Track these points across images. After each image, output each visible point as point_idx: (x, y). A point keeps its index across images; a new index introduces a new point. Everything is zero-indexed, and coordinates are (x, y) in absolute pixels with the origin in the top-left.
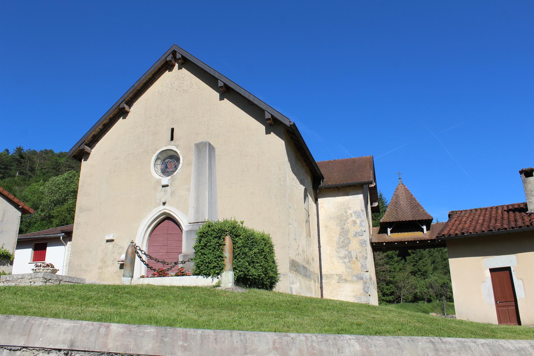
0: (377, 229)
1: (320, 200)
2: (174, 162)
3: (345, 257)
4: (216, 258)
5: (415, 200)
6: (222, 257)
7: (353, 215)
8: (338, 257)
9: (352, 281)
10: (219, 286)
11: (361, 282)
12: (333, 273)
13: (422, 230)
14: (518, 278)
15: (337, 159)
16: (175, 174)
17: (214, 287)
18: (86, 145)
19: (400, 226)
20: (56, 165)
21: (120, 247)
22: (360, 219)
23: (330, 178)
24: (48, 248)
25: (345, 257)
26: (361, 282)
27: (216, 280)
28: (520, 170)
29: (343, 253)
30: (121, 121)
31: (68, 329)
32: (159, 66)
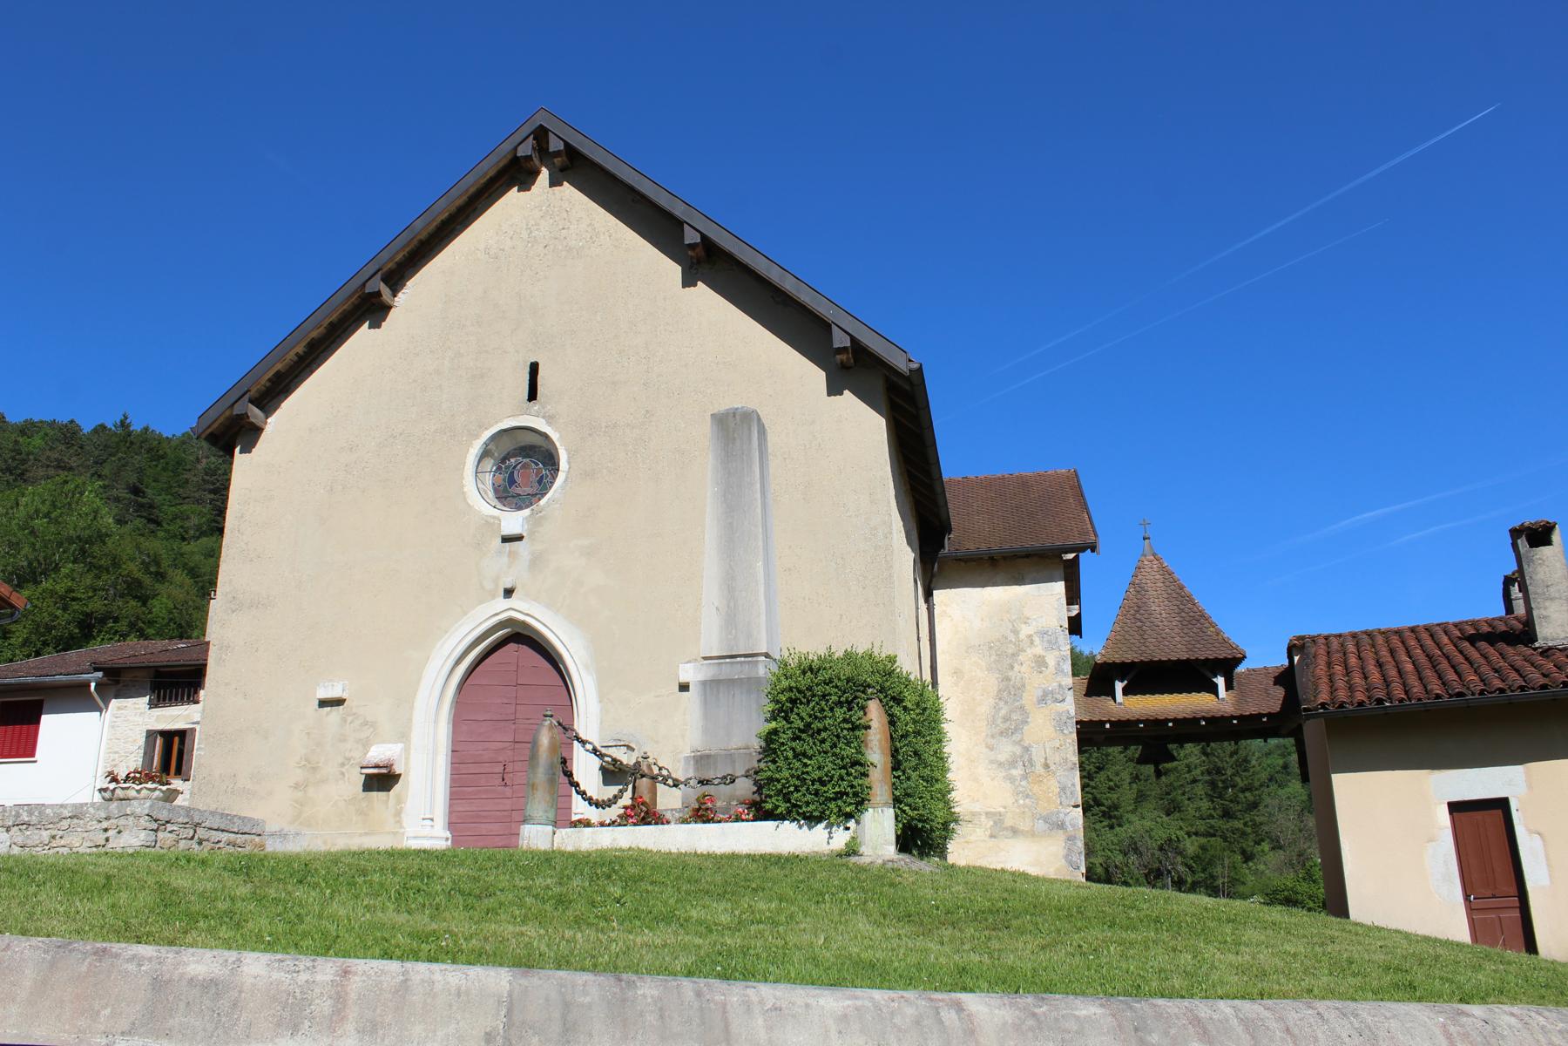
0: (1083, 680)
1: (938, 595)
2: (536, 468)
3: (1012, 763)
4: (844, 767)
5: (1191, 600)
6: (861, 765)
7: (1037, 640)
8: (992, 762)
9: (1032, 834)
10: (855, 853)
11: (1060, 837)
12: (977, 808)
13: (1213, 689)
14: (1530, 832)
15: (972, 477)
16: (543, 501)
17: (840, 855)
18: (251, 401)
19: (1149, 676)
20: (14, 459)
21: (366, 723)
22: (1056, 653)
23: (969, 529)
24: (44, 718)
25: (1012, 763)
26: (1060, 837)
27: (840, 838)
28: (1517, 525)
29: (1007, 749)
30: (363, 335)
31: (844, 1018)
32: (491, 173)
